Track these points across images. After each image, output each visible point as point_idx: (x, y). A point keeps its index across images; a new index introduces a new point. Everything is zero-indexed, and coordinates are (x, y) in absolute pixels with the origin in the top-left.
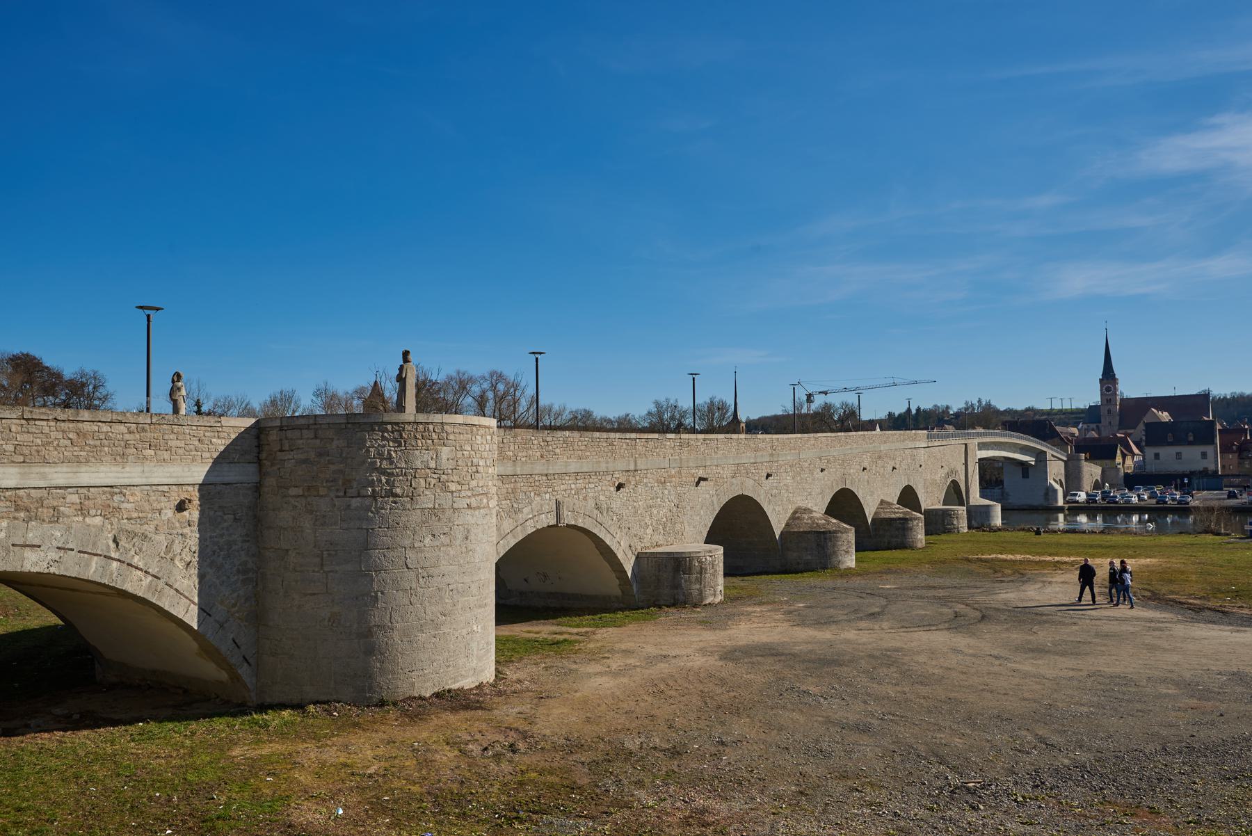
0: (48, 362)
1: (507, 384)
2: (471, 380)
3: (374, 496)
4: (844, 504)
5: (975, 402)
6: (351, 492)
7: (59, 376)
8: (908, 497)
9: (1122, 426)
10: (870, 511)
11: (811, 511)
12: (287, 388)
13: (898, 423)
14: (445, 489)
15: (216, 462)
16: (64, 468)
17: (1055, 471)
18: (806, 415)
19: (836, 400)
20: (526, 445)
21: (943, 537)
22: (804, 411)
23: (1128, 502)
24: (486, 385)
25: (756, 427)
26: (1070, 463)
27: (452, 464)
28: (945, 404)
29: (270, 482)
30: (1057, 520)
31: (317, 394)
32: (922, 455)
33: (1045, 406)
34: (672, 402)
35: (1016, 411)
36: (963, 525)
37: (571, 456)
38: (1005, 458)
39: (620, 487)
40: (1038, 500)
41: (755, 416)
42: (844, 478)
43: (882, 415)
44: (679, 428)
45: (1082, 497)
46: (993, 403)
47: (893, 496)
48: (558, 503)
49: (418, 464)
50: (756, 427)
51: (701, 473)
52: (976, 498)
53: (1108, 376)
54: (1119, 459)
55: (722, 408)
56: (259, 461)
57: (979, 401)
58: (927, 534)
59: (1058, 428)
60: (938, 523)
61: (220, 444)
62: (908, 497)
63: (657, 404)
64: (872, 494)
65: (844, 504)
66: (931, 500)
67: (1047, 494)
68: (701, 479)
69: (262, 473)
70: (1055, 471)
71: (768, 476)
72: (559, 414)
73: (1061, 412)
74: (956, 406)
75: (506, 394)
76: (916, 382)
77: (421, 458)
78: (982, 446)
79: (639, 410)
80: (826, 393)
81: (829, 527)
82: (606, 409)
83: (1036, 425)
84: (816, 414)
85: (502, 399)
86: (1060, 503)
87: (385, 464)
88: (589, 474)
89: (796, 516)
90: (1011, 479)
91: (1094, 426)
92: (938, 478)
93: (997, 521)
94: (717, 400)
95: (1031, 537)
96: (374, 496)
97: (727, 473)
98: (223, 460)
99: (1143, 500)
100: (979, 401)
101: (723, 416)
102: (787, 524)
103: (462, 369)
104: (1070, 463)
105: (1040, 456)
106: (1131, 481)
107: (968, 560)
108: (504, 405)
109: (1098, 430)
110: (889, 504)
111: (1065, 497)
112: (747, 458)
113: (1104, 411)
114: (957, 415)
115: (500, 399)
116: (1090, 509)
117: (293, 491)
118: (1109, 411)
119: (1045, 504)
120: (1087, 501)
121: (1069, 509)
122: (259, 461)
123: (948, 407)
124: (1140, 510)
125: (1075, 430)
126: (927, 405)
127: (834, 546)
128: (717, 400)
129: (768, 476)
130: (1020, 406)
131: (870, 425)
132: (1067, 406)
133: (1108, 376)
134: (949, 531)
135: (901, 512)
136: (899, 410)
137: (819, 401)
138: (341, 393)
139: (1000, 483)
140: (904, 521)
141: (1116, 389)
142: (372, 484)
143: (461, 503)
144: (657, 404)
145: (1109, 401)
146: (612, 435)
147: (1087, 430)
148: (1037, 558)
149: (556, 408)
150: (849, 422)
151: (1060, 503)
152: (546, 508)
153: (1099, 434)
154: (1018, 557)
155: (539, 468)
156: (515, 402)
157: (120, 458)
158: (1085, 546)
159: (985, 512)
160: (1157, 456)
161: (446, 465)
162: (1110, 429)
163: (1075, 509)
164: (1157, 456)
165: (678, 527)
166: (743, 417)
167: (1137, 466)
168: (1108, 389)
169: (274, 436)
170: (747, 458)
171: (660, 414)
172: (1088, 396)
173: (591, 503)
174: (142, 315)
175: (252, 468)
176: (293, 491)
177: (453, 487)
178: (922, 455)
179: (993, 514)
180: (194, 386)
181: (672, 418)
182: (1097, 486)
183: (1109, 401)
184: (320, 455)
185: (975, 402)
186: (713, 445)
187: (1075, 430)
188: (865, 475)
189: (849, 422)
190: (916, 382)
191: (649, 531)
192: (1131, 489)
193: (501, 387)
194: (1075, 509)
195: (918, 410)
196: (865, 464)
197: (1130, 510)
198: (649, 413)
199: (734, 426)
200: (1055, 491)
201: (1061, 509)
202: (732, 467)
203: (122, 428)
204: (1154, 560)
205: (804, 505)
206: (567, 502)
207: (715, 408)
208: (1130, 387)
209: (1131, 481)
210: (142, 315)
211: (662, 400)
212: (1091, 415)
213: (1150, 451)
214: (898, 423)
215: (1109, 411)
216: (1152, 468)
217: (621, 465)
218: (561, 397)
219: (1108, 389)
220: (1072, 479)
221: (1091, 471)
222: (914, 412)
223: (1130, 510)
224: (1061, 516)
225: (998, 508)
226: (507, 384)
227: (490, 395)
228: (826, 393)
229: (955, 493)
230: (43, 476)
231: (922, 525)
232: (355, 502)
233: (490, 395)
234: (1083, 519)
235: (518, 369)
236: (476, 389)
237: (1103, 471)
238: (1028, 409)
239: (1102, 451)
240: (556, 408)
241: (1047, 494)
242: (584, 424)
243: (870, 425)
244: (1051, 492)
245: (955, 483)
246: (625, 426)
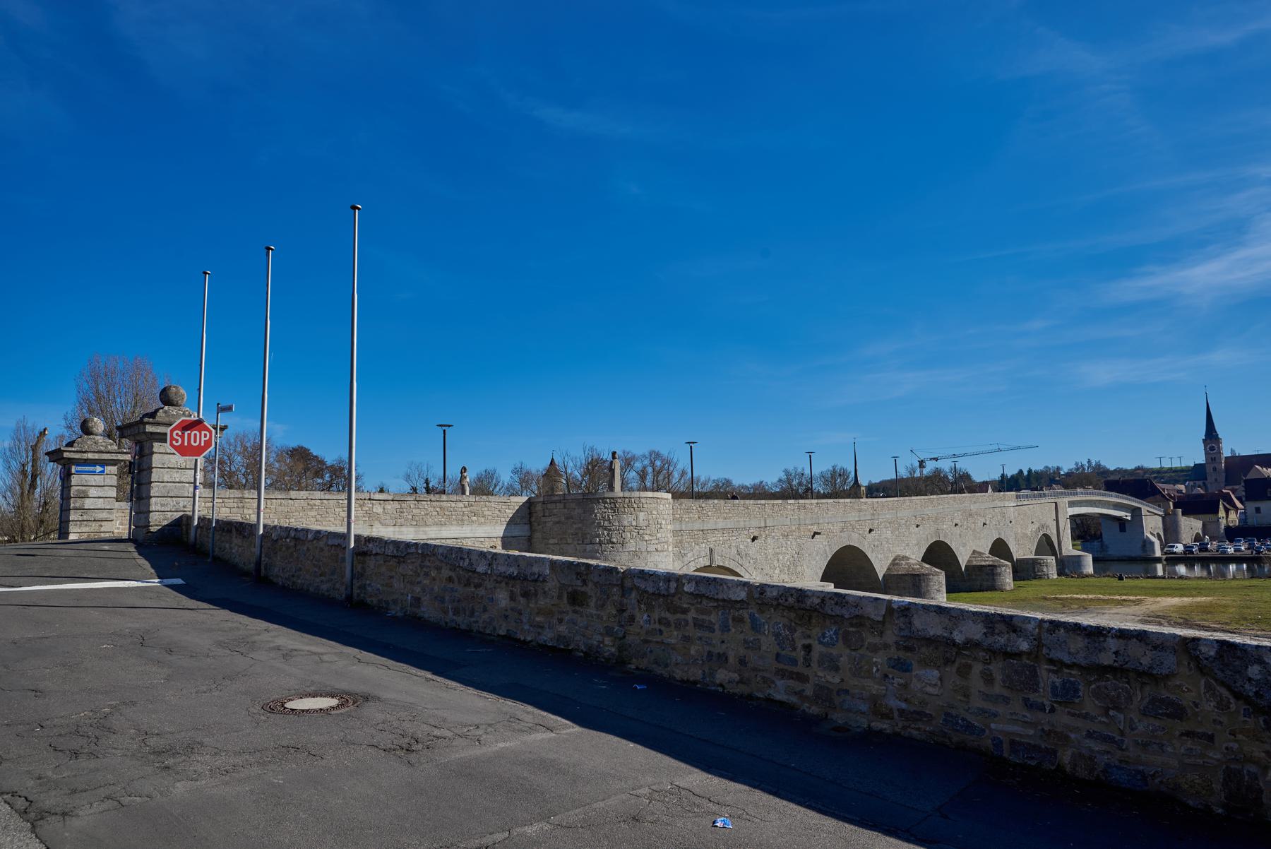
0: (314, 452)
1: (663, 461)
2: (633, 458)
3: (600, 543)
4: (939, 554)
5: (1085, 463)
6: (587, 541)
7: (322, 462)
8: (1000, 548)
9: (1228, 482)
10: (963, 561)
11: (907, 558)
12: (490, 467)
13: (1009, 484)
14: (642, 539)
15: (509, 524)
16: (434, 528)
17: (1152, 524)
18: (919, 479)
19: (946, 466)
20: (689, 510)
21: (1034, 582)
22: (917, 474)
23: (1224, 552)
24: (646, 462)
25: (874, 491)
26: (1167, 518)
27: (646, 523)
28: (1055, 465)
29: (538, 535)
30: (1155, 569)
31: (515, 472)
32: (1011, 513)
33: (1155, 465)
34: (800, 470)
35: (1126, 471)
36: (1053, 572)
37: (718, 515)
38: (1101, 515)
39: (754, 539)
40: (1137, 552)
41: (876, 480)
42: (937, 532)
43: (996, 476)
44: (808, 493)
45: (1179, 548)
46: (1103, 463)
47: (985, 547)
48: (711, 550)
49: (626, 523)
50: (874, 491)
51: (815, 529)
52: (1068, 548)
53: (1211, 436)
54: (1222, 513)
55: (843, 474)
56: (530, 523)
57: (1089, 462)
58: (1014, 580)
59: (1160, 486)
60: (1025, 571)
61: (510, 513)
62: (1000, 548)
63: (787, 472)
64: (964, 545)
65: (939, 554)
66: (1022, 550)
67: (1144, 546)
68: (816, 533)
69: (532, 530)
70: (1152, 524)
71: (871, 531)
72: (705, 484)
73: (1171, 470)
74: (1067, 466)
75: (662, 468)
76: (1019, 448)
77: (627, 519)
78: (1072, 504)
79: (771, 478)
80: (936, 459)
81: (923, 571)
82: (743, 478)
83: (1139, 485)
84: (927, 478)
85: (659, 472)
86: (1158, 553)
87: (606, 524)
88: (732, 530)
89: (895, 563)
90: (1110, 534)
91: (1200, 483)
92: (1029, 532)
93: (1089, 568)
94: (838, 469)
95: (1115, 582)
96: (600, 543)
97: (836, 528)
98: (511, 523)
99: (1240, 550)
100: (1089, 462)
101: (844, 482)
102: (889, 569)
103: (627, 450)
104: (1167, 518)
105: (1136, 512)
106: (1232, 534)
107: (1045, 599)
108: (661, 477)
109: (1205, 486)
110: (980, 553)
111: (1162, 549)
112: (853, 516)
113: (1209, 469)
114: (1069, 474)
115: (657, 473)
116: (1188, 559)
117: (552, 541)
118: (1215, 469)
119: (1143, 555)
120: (1184, 552)
121: (1167, 559)
122: (530, 523)
123: (1058, 468)
124: (1237, 560)
125: (1182, 487)
126: (1038, 467)
127: (928, 586)
128: (838, 469)
129: (871, 531)
130: (1130, 465)
131: (982, 487)
132: (1176, 464)
133: (1211, 436)
134: (1040, 577)
135: (991, 560)
136: (1011, 472)
137: (930, 467)
138: (533, 471)
139: (1099, 537)
140: (993, 567)
141: (1219, 448)
142: (598, 536)
143: (652, 548)
144: (787, 472)
145: (1213, 460)
146: (747, 502)
147: (1194, 487)
148: (1106, 597)
149: (702, 479)
150: (962, 484)
151: (1158, 553)
152: (703, 554)
153: (1206, 490)
154: (1090, 596)
155: (698, 526)
156: (669, 475)
157: (461, 522)
158: (1182, 589)
159: (1077, 561)
160: (1258, 510)
161: (642, 523)
162: (1215, 485)
163: (1173, 560)
164: (1258, 510)
165: (799, 569)
166: (864, 482)
167: (1244, 519)
168: (1212, 449)
169: (539, 507)
170: (853, 516)
171: (789, 481)
172: (1195, 455)
173: (734, 551)
174: (440, 430)
175: (527, 527)
176: (552, 541)
177: (647, 538)
178: (1011, 513)
179: (1084, 563)
180: (424, 468)
181: (800, 484)
182: (1197, 538)
183: (1213, 460)
184: (567, 518)
185: (1085, 463)
186: (824, 507)
187: (1182, 487)
188: (957, 530)
189: (962, 484)
190: (1019, 448)
191: (777, 571)
192: (1231, 541)
193: (658, 463)
194: (1173, 560)
195: (1030, 471)
196: (957, 521)
197: (1226, 560)
198: (780, 480)
199: (854, 491)
200: (1152, 543)
201: (1158, 560)
202: (842, 524)
203: (461, 505)
204: (1185, 599)
205: (899, 553)
206: (717, 550)
207: (836, 475)
208: (1235, 444)
209: (1232, 534)
210: (440, 430)
211: (791, 468)
212: (1197, 473)
213: (1252, 506)
214: (1009, 484)
215: (1215, 469)
216: (1253, 521)
217: (755, 523)
218: (708, 472)
219: (1212, 449)
220: (1171, 533)
221: (1190, 526)
222: (1026, 473)
223: (1226, 560)
224: (1159, 567)
225: (1089, 559)
226: (663, 461)
227: (650, 470)
228: (936, 459)
229: (1047, 545)
230: (425, 533)
231: (1009, 570)
232: (589, 547)
233: (650, 470)
234: (1182, 569)
235: (673, 449)
236: (638, 465)
237: (1204, 525)
238: (1138, 469)
239: (1199, 506)
240: (702, 479)
241: (1144, 546)
242: (726, 493)
243: (982, 487)
244: (1148, 544)
245: (1047, 537)
246: (759, 493)
